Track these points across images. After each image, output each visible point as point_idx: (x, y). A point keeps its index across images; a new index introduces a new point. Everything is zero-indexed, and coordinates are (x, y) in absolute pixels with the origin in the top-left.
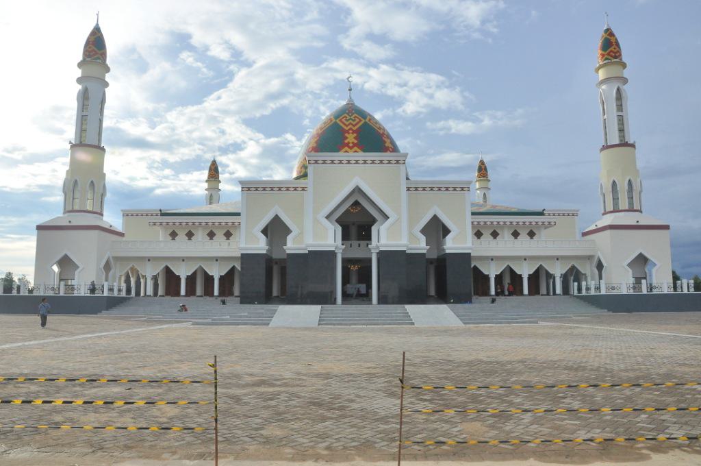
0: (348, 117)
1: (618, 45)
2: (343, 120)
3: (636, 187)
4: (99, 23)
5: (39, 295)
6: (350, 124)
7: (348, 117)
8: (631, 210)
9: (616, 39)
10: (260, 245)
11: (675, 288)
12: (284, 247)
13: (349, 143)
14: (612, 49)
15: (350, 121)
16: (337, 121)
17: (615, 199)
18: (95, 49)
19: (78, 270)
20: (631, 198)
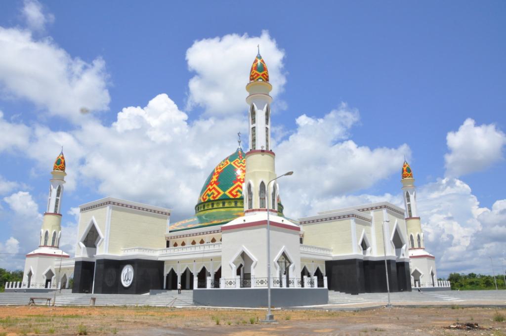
0: (240, 161)
1: (64, 164)
2: (236, 163)
3: (58, 236)
4: (260, 53)
5: (235, 288)
6: (241, 165)
7: (240, 161)
8: (53, 246)
9: (64, 161)
10: (81, 253)
11: (46, 286)
12: (94, 255)
13: (240, 179)
14: (61, 165)
15: (241, 164)
16: (232, 163)
17: (46, 241)
18: (257, 72)
19: (421, 276)
20: (419, 243)
